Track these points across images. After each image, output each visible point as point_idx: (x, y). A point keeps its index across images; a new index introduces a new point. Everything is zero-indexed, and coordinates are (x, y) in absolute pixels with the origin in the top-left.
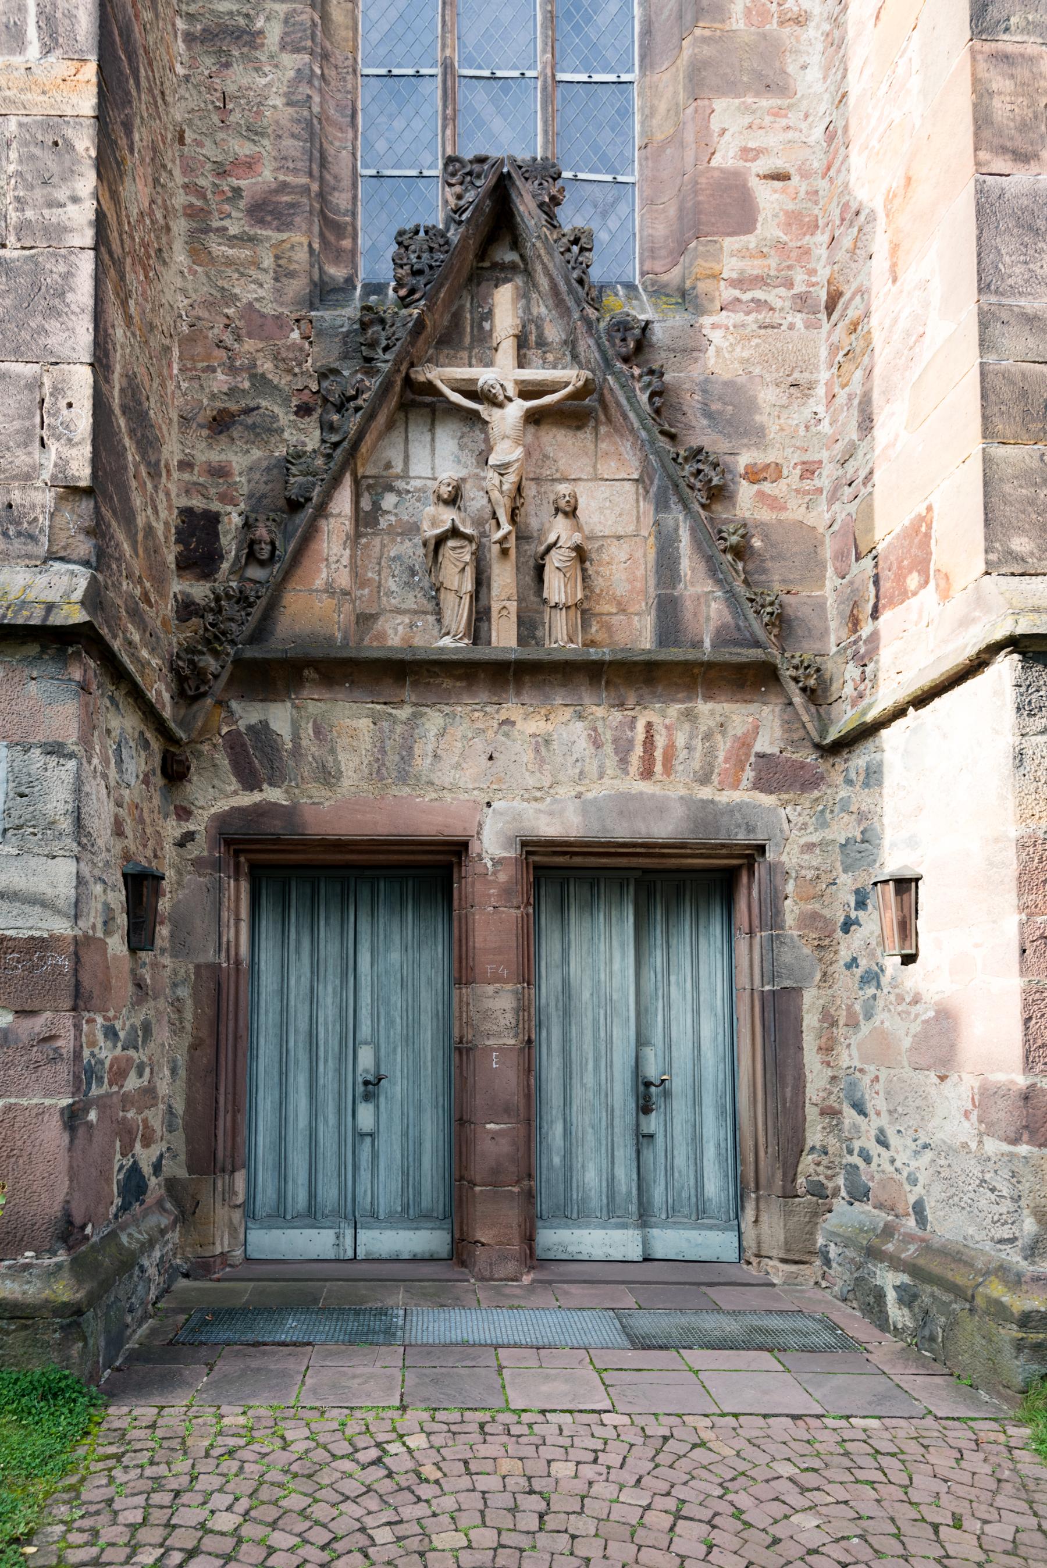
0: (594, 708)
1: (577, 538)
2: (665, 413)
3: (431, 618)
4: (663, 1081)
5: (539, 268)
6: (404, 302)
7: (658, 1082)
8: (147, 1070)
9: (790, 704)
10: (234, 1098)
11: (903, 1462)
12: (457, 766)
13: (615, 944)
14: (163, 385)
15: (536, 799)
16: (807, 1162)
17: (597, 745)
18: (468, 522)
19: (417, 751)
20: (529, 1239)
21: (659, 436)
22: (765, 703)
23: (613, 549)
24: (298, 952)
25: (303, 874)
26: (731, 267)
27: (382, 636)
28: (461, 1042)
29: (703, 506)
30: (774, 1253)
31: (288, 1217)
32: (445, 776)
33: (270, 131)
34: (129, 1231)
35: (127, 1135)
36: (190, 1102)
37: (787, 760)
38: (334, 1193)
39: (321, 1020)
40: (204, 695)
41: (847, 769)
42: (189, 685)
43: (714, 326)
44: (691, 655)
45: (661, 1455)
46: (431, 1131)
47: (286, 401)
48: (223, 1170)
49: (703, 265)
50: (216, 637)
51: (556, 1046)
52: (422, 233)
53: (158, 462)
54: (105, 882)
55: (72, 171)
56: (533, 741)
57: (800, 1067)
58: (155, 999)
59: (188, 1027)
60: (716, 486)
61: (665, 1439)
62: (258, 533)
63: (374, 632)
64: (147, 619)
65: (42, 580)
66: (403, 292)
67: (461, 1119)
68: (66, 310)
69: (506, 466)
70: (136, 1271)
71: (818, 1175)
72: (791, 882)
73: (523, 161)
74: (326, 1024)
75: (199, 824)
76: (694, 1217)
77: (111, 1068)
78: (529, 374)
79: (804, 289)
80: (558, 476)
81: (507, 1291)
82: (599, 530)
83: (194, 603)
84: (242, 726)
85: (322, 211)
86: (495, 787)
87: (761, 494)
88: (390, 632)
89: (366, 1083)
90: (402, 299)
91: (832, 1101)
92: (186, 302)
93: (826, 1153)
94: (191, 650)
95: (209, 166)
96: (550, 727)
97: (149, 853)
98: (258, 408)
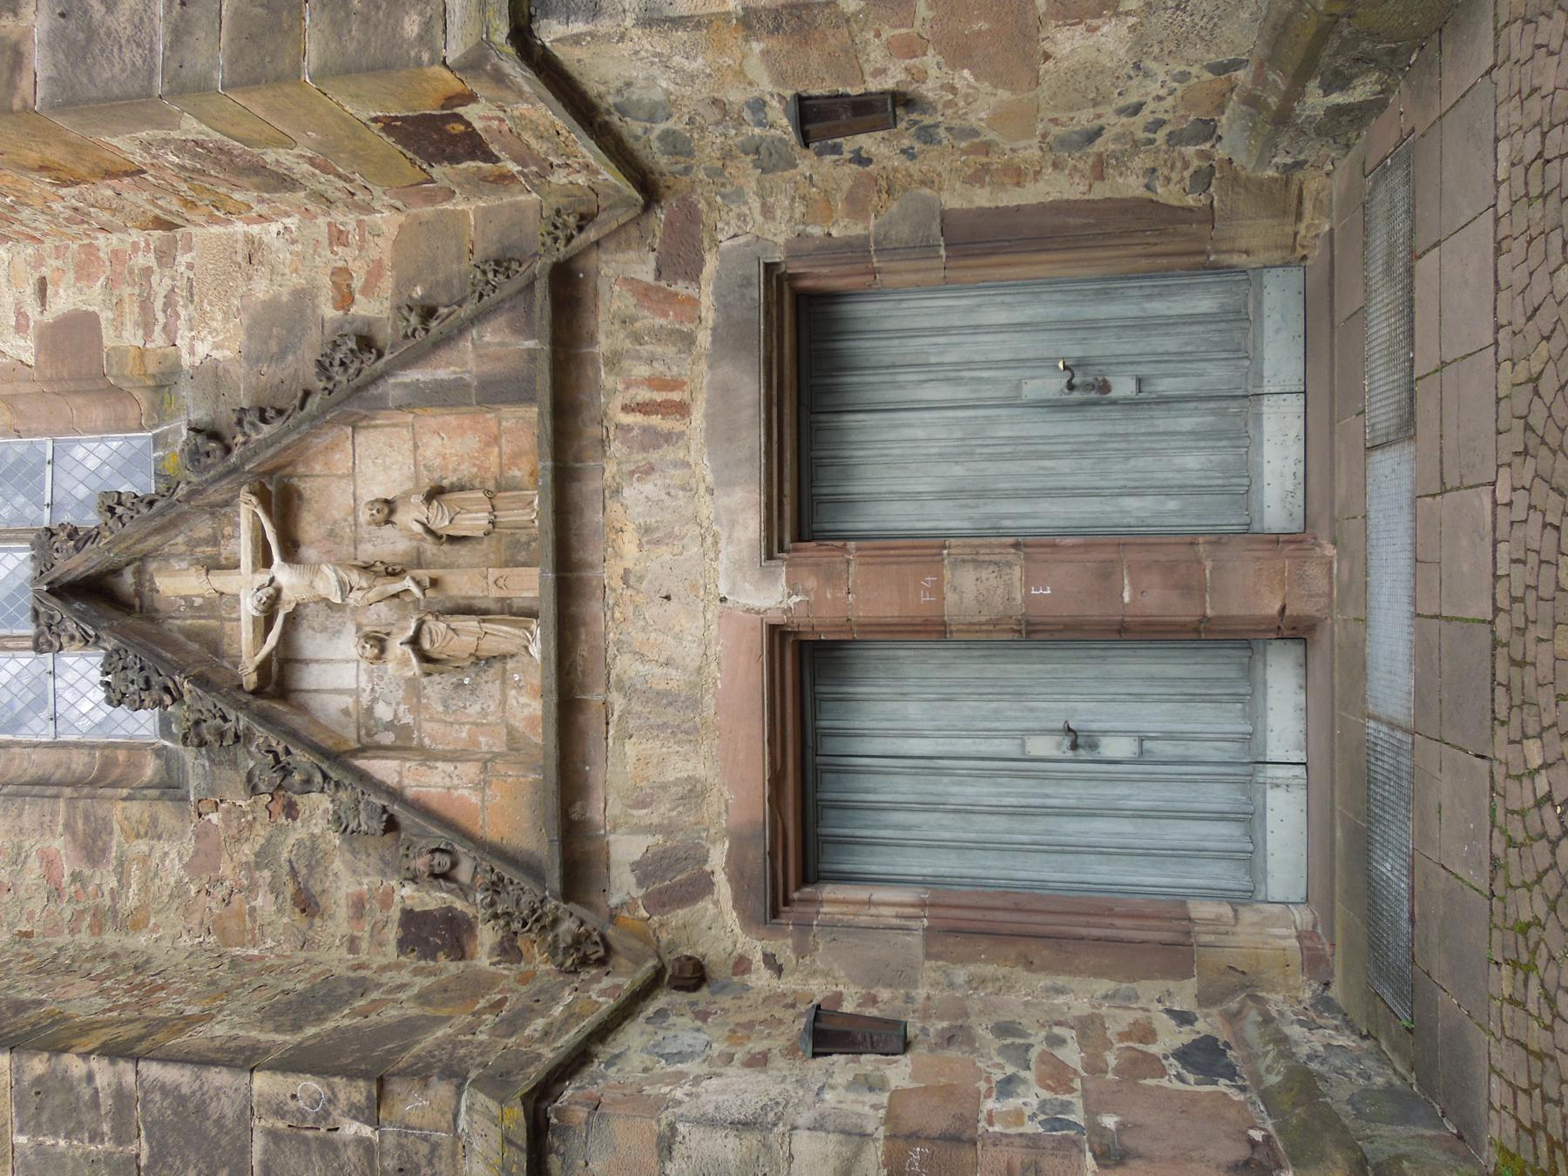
0: (607, 474)
1: (417, 499)
2: (280, 404)
3: (510, 664)
4: (1065, 368)
5: (139, 547)
6: (177, 698)
7: (1068, 373)
8: (1056, 1030)
9: (597, 243)
10: (1096, 915)
11: (1553, 126)
12: (678, 638)
13: (892, 436)
14: (270, 969)
15: (716, 543)
16: (1166, 194)
17: (650, 470)
18: (404, 624)
19: (662, 686)
20: (1276, 540)
21: (306, 410)
22: (598, 272)
23: (428, 453)
24: (909, 828)
25: (803, 838)
26: (132, 337)
27: (530, 720)
28: (1019, 632)
29: (380, 355)
30: (1289, 230)
31: (1251, 847)
32: (690, 653)
33: (16, 840)
34: (1262, 1071)
35: (1140, 1065)
36: (1099, 973)
37: (663, 242)
38: (1218, 788)
39: (994, 801)
40: (603, 937)
41: (672, 174)
42: (588, 954)
43: (192, 352)
44: (544, 365)
45: (1548, 439)
46: (1135, 665)
47: (282, 829)
48: (1188, 933)
49: (131, 368)
50: (537, 920)
51: (1024, 507)
52: (109, 678)
53: (351, 981)
54: (822, 1088)
55: (63, 1078)
56: (647, 547)
57: (1042, 208)
58: (967, 1015)
59: (1004, 970)
60: (357, 343)
61: (1528, 427)
62: (422, 868)
63: (528, 732)
64: (519, 1006)
65: (478, 1145)
66: (167, 699)
67: (1119, 632)
68: (198, 1094)
69: (341, 583)
70: (1314, 1066)
71: (1182, 179)
72: (809, 229)
73: (35, 569)
74: (999, 795)
75: (755, 949)
76: (1246, 325)
77: (1048, 1088)
78: (246, 558)
79: (152, 255)
80: (351, 519)
81: (1345, 576)
82: (409, 470)
83: (501, 943)
84: (638, 893)
85: (91, 784)
86: (702, 592)
87: (365, 291)
88: (526, 712)
89: (1074, 746)
90: (174, 700)
91: (1086, 166)
92: (185, 937)
93: (1154, 170)
94: (553, 949)
95: (52, 907)
96: (630, 527)
97: (789, 1015)
98: (290, 861)
